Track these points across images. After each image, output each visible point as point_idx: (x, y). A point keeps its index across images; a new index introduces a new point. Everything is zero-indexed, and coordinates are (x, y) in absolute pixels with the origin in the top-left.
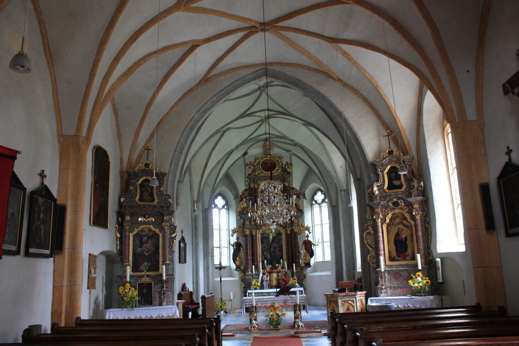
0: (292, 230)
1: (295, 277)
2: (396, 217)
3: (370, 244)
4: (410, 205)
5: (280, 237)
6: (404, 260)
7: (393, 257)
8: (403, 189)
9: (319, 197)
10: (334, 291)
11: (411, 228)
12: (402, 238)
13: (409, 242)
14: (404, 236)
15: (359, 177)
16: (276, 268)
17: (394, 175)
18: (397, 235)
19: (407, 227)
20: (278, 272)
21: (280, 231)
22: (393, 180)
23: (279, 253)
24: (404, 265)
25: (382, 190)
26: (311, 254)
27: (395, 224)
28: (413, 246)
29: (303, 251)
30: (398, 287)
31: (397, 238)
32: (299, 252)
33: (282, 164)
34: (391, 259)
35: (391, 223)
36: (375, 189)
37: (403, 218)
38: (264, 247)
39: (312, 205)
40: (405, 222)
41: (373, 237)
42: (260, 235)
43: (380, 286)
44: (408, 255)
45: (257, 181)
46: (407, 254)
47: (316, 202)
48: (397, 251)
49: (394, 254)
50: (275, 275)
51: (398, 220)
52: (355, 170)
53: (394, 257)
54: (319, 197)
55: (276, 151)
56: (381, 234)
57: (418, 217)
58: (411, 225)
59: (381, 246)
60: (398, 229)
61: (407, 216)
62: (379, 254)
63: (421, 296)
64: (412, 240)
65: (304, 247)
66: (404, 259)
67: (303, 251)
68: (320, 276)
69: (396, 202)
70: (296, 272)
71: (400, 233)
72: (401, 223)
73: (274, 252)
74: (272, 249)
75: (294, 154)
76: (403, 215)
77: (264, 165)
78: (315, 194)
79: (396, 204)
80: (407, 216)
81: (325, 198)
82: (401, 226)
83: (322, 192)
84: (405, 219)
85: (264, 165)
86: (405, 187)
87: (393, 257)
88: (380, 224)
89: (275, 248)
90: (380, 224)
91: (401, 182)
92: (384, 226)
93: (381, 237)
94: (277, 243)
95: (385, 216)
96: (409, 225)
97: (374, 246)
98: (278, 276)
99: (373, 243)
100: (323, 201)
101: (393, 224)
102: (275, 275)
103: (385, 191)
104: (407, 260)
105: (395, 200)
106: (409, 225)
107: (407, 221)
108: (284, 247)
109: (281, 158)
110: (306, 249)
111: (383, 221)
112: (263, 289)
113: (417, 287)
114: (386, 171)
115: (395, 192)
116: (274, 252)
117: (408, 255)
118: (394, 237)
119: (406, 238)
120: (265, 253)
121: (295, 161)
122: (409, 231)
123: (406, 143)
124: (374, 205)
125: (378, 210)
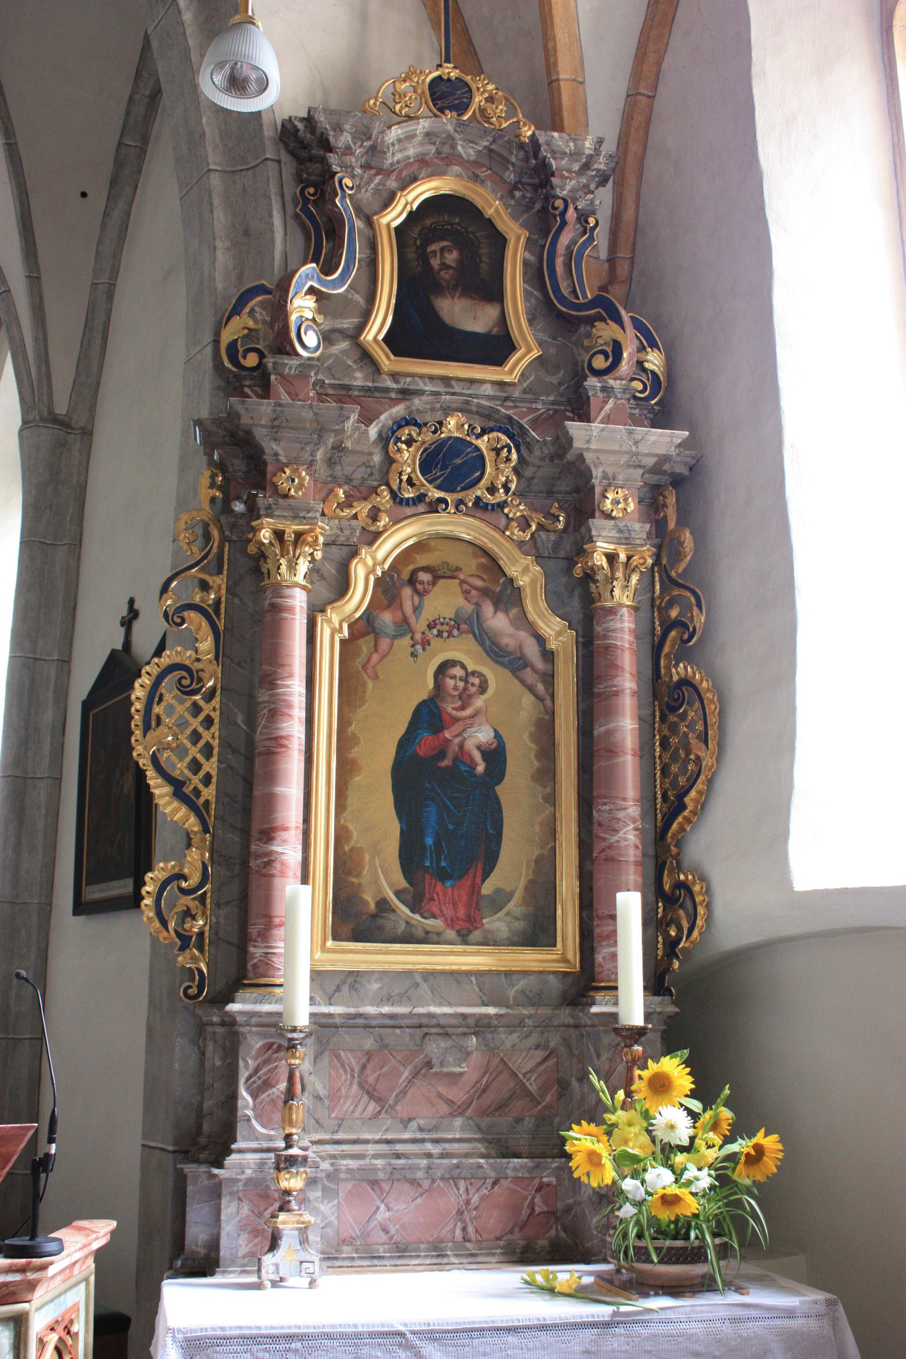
2: (437, 574)
3: (180, 768)
4: (572, 495)
6: (464, 938)
7: (370, 900)
8: (514, 370)
10: (662, 1141)
11: (549, 679)
12: (462, 754)
13: (516, 793)
14: (482, 735)
15: (61, 408)
17: (452, 257)
18: (429, 716)
19: (515, 663)
22: (438, 289)
24: (457, 976)
25: (344, 345)
27: (420, 626)
28: (552, 833)
30: (397, 1176)
31: (425, 744)
34: (353, 918)
35: (387, 618)
36: (302, 306)
37: (485, 592)
40: (498, 621)
41: (212, 708)
43: (243, 1161)
44: (498, 901)
46: (487, 888)
48: (410, 855)
49: (384, 877)
51: (444, 602)
52: (44, 359)
53: (383, 905)
56: (295, 688)
57: (623, 595)
58: (549, 656)
59: (291, 790)
60: (443, 669)
61: (525, 572)
62: (616, 667)
63: (706, 1285)
64: (547, 773)
66: (466, 931)
69: (457, 446)
71: (449, 707)
72: (468, 625)
76: (492, 565)
79: (451, 466)
80: (525, 572)
82: (464, 652)
84: (507, 595)
86: (527, 354)
87: (370, 900)
88: (298, 600)
90: (298, 600)
91: (503, 319)
92: (324, 633)
93: (298, 712)
95: (344, 554)
96: (532, 650)
97: (209, 793)
99: (211, 766)
101: (404, 626)
103: (366, 357)
104: (489, 941)
105: (453, 425)
106: (532, 650)
107: (523, 621)
111: (324, 592)
113: (669, 1201)
114: (394, 216)
115: (446, 380)
117: (498, 901)
118: (401, 729)
119: (495, 756)
122: (528, 700)
123: (564, 72)
124: (276, 427)
125: (298, 482)
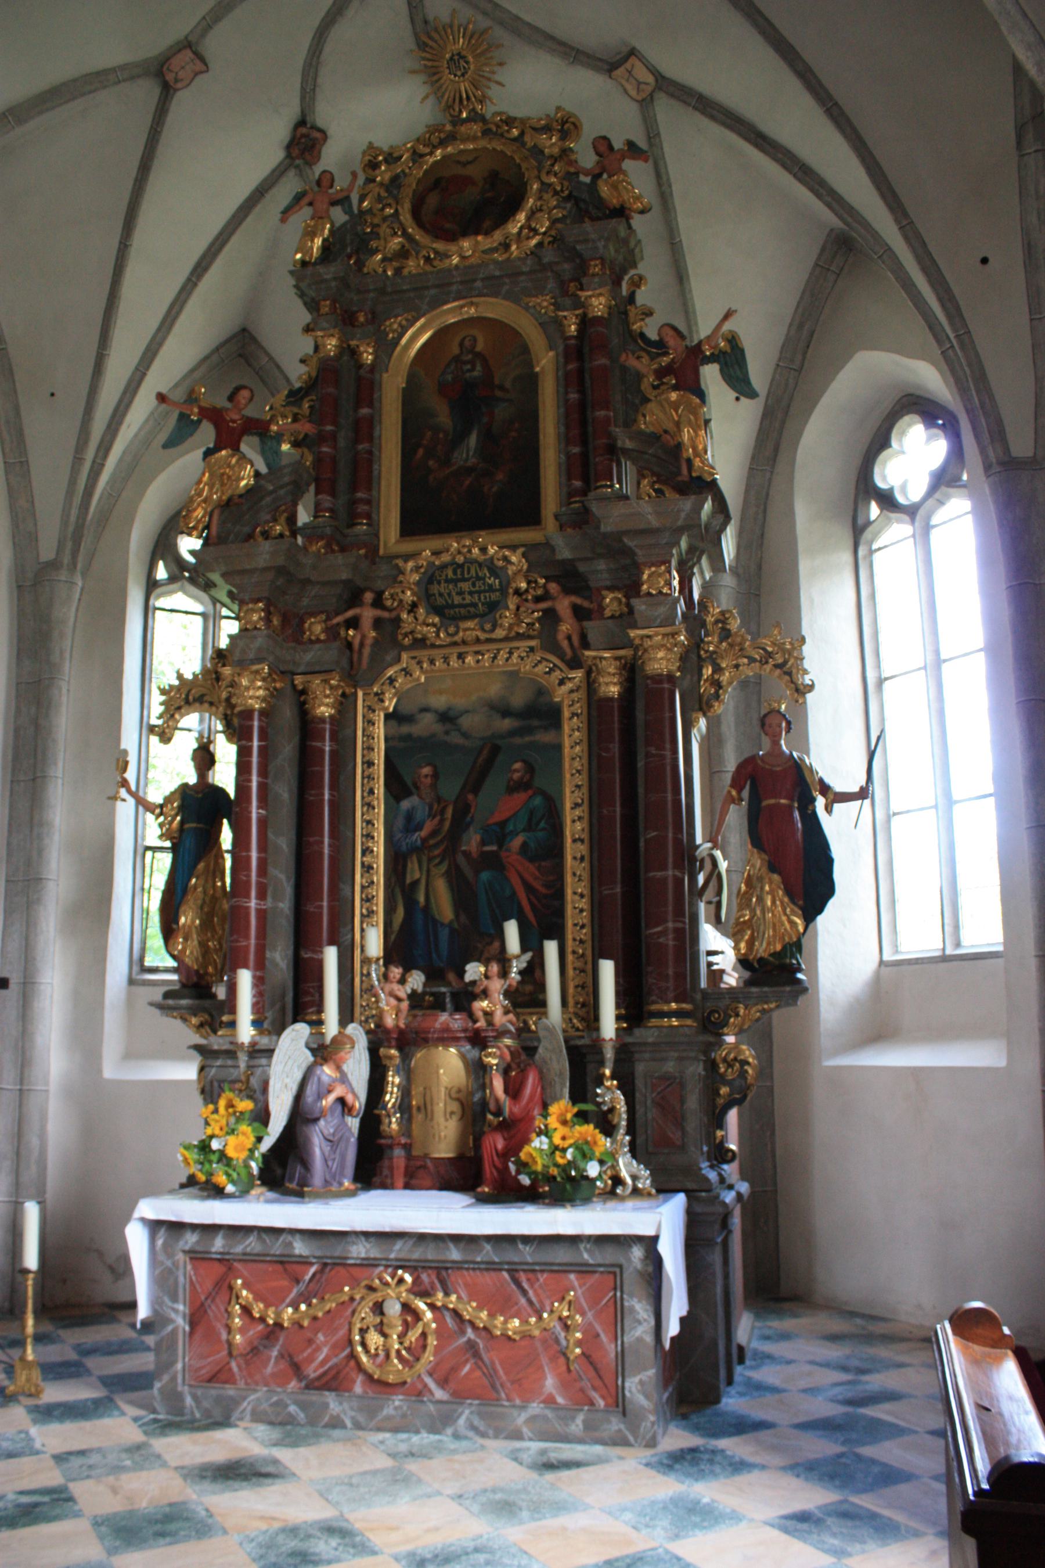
0: (632, 672)
1: (611, 1095)
5: (546, 737)
9: (914, 456)
16: (464, 998)
20: (478, 1040)
21: (541, 691)
23: (530, 870)
26: (809, 879)
29: (726, 854)
32: (687, 858)
33: (571, 176)
38: (411, 824)
39: (858, 531)
42: (380, 730)
45: (375, 318)
47: (887, 500)
50: (449, 1065)
54: (914, 456)
55: (527, 86)
65: (736, 817)
67: (726, 854)
68: (916, 1073)
70: (625, 1052)
73: (492, 862)
74: (472, 841)
75: (665, 85)
77: (433, 200)
78: (880, 442)
81: (957, 453)
83: (929, 411)
85: (433, 200)
89: (499, 834)
94: (514, 788)
98: (478, 1070)
100: (943, 480)
102: (449, 1065)
108: (574, 825)
109: (566, 126)
110: (756, 838)
112: (299, 1194)
116: (492, 862)
120: (414, 871)
121: (694, 151)
